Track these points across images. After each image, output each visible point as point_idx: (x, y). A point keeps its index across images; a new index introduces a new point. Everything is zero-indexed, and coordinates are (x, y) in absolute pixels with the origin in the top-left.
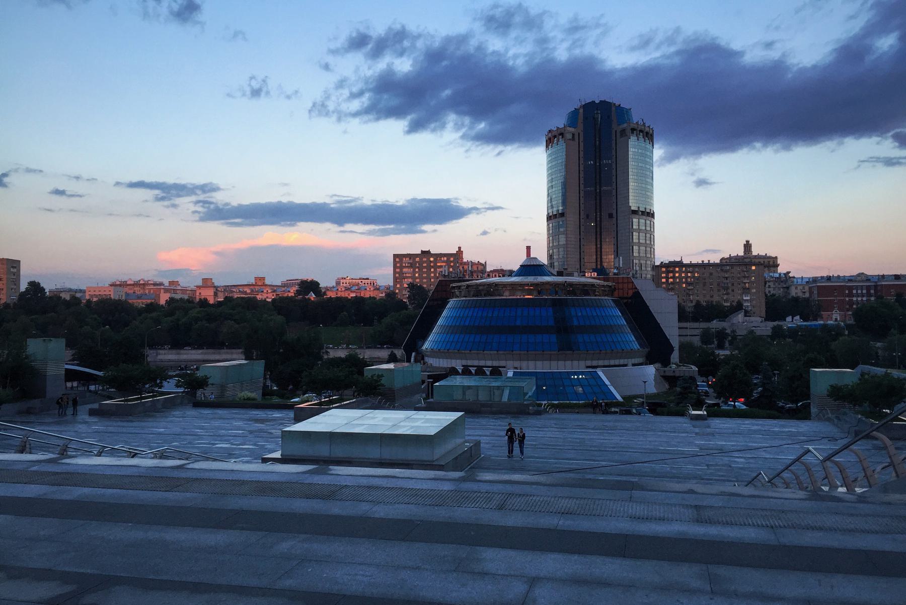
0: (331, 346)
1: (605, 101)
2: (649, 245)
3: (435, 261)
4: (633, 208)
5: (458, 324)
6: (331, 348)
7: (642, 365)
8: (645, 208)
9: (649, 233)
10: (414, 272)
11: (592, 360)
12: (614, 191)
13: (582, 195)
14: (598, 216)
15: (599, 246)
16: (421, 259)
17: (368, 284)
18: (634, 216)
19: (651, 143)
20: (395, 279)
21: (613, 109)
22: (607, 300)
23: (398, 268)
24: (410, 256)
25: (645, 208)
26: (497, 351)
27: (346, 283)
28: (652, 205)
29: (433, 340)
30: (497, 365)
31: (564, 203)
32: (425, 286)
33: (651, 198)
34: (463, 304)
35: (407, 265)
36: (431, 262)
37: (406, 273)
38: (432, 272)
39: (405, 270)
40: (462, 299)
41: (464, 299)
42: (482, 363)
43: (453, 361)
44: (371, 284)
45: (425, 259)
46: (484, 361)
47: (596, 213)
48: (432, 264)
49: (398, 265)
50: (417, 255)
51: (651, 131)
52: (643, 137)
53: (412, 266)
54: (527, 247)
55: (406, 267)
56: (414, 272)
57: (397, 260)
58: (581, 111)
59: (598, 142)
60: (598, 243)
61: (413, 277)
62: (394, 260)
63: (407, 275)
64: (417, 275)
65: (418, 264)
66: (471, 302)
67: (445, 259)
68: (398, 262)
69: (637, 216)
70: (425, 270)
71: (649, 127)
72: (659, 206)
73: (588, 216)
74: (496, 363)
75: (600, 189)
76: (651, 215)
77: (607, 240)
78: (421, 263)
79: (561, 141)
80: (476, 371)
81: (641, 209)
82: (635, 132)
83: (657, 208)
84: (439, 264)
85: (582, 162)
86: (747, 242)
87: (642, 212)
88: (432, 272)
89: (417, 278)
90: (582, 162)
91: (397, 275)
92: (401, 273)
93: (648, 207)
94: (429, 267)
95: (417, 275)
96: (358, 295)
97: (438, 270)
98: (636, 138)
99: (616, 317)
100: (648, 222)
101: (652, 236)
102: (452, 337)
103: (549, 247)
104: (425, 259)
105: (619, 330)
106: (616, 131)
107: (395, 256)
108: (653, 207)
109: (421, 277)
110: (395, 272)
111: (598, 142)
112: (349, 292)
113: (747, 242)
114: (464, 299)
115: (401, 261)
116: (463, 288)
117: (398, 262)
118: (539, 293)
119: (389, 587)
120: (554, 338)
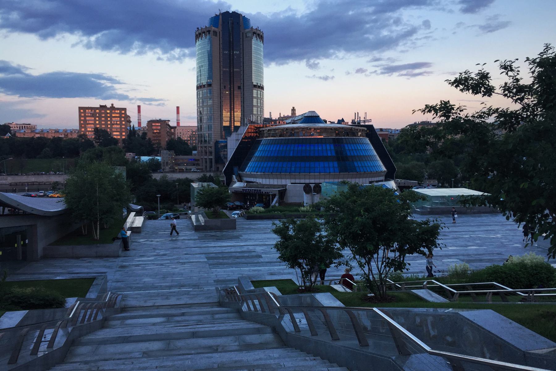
0: (44, 173)
1: (235, 12)
2: (261, 107)
3: (111, 113)
4: (254, 84)
5: (260, 155)
6: (44, 174)
7: (382, 182)
8: (257, 83)
9: (261, 99)
10: (95, 120)
11: (329, 179)
12: (242, 72)
13: (221, 73)
14: (232, 87)
15: (232, 107)
16: (100, 111)
17: (17, 127)
18: (255, 88)
19: (261, 41)
20: (80, 124)
21: (241, 18)
22: (350, 140)
23: (82, 117)
24: (91, 108)
25: (257, 83)
26: (280, 173)
27: (15, 127)
28: (262, 81)
29: (251, 166)
30: (319, 182)
31: (210, 77)
32: (109, 130)
33: (262, 77)
34: (264, 142)
35: (89, 115)
36: (108, 113)
37: (89, 121)
38: (109, 121)
39: (87, 118)
40: (269, 138)
41: (272, 138)
42: (307, 181)
43: (279, 180)
44: (20, 127)
45: (103, 126)
46: (304, 180)
47: (230, 85)
48: (108, 115)
49: (83, 115)
50: (97, 108)
51: (261, 34)
52: (256, 37)
53: (93, 115)
54: (79, 107)
55: (88, 116)
56: (95, 120)
57: (82, 111)
58: (221, 17)
59: (231, 39)
60: (232, 105)
61: (95, 124)
62: (80, 112)
63: (90, 122)
64: (97, 122)
65: (98, 115)
66: (269, 141)
67: (118, 111)
68: (82, 113)
69: (257, 89)
70: (103, 119)
71: (260, 30)
72: (266, 84)
73: (225, 87)
74: (317, 181)
75: (233, 70)
76: (262, 88)
77: (237, 103)
78: (100, 114)
79: (206, 35)
80: (314, 187)
81: (259, 85)
82: (255, 35)
83: (265, 84)
84: (113, 115)
85: (221, 51)
86: (293, 108)
87: (259, 86)
88: (109, 121)
89: (97, 124)
90: (221, 51)
91: (82, 122)
92: (85, 121)
93: (261, 83)
94: (106, 117)
95: (97, 122)
96: (42, 136)
97: (113, 119)
98: (256, 38)
99: (363, 151)
100: (259, 92)
101: (262, 101)
102: (257, 164)
103: (198, 107)
104: (103, 126)
105: (364, 159)
106: (243, 33)
107: (80, 108)
108: (263, 83)
109: (100, 124)
110: (80, 120)
111: (231, 39)
112: (35, 134)
113: (293, 108)
114: (272, 138)
115: (85, 112)
116: (265, 131)
117: (82, 113)
118: (337, 135)
119: (498, 323)
120: (336, 164)
